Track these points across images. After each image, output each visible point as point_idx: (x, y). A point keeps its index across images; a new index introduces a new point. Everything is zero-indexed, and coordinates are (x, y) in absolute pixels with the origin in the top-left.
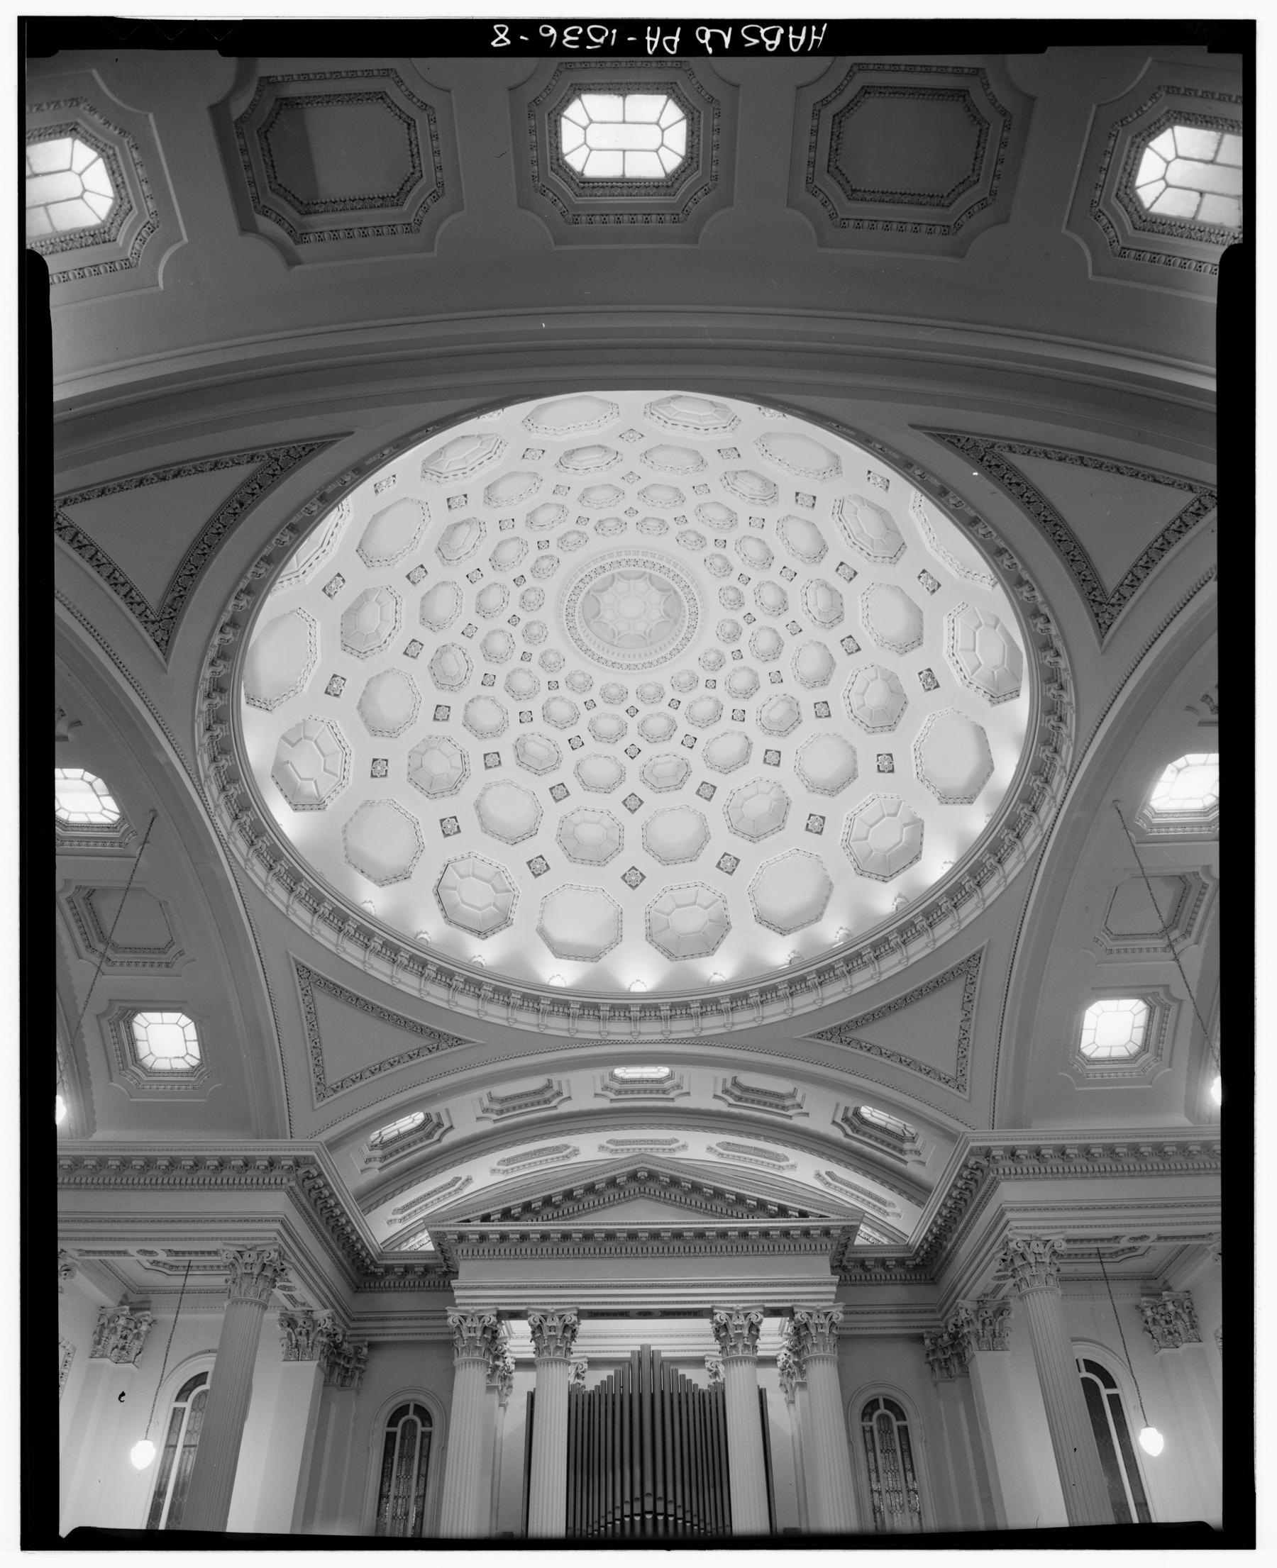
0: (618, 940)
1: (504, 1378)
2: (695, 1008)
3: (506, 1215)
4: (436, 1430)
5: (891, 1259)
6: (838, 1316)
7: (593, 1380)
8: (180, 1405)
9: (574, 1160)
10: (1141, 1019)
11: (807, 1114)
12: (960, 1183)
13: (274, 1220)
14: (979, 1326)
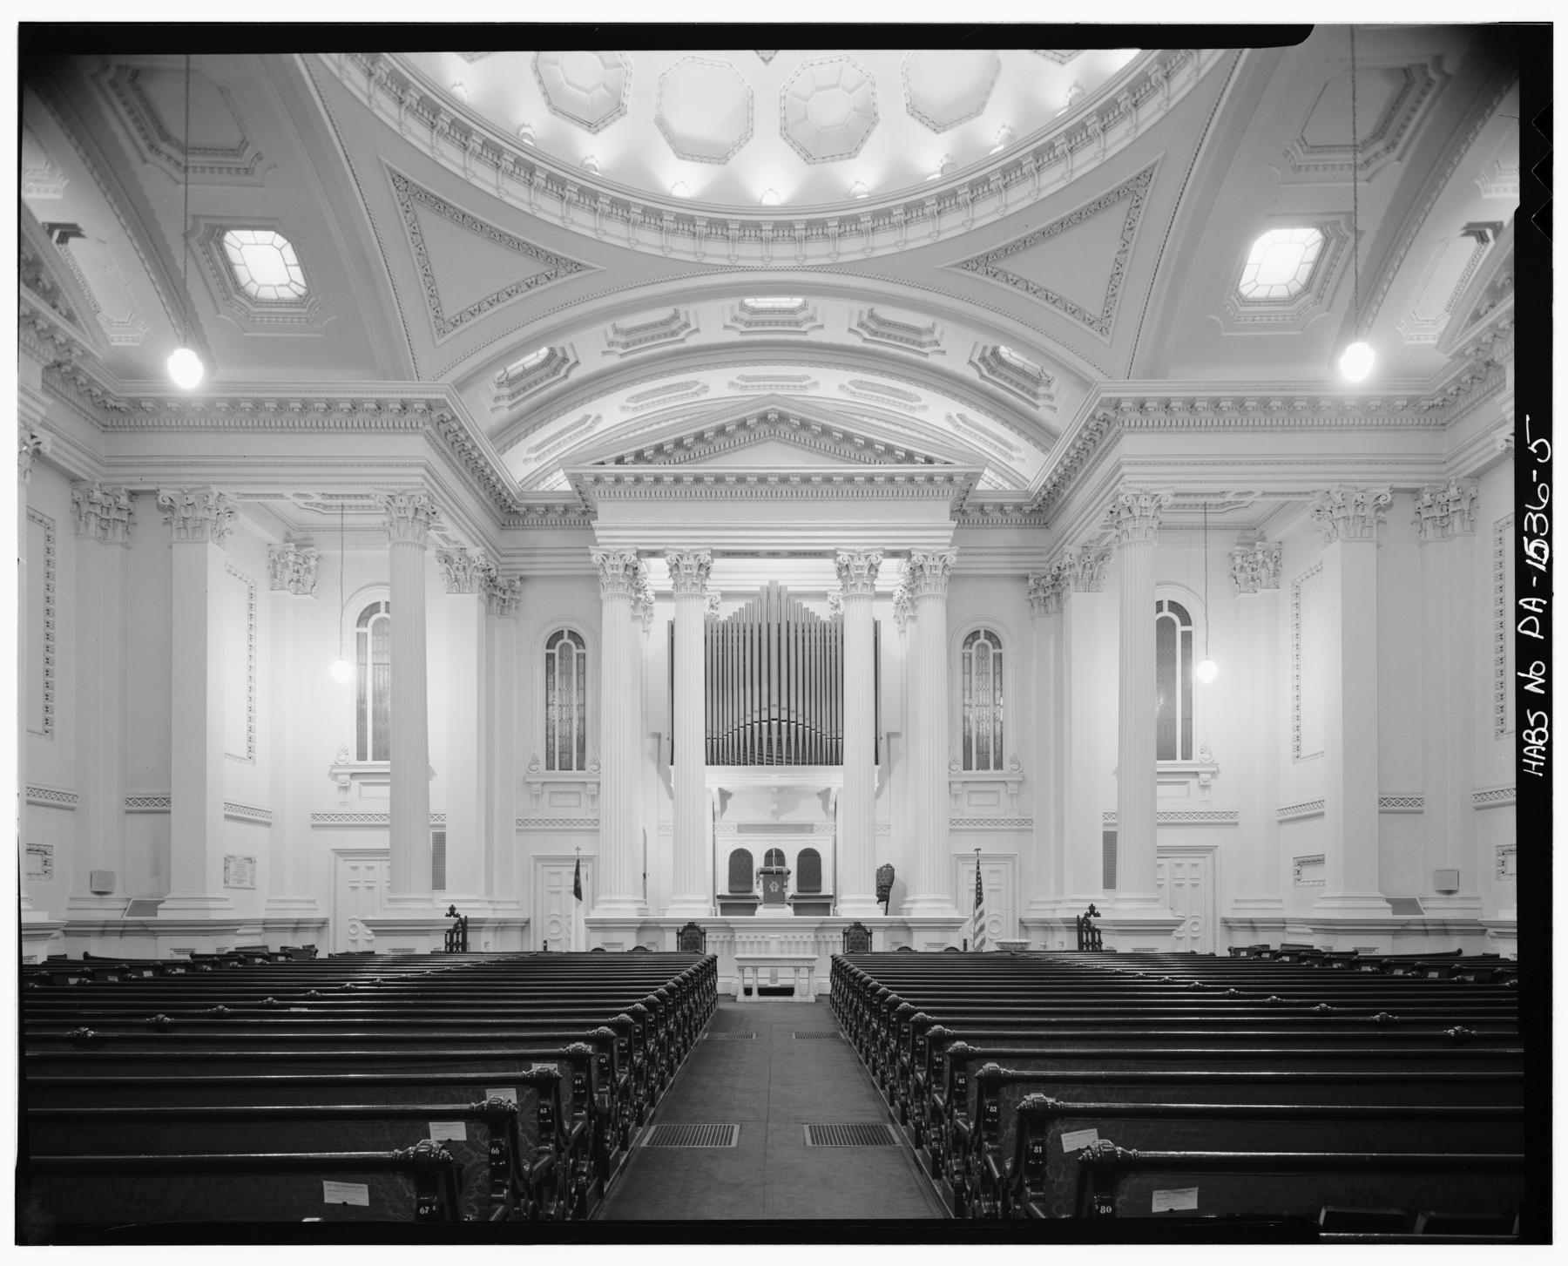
0: (747, 136)
1: (646, 608)
2: (833, 228)
3: (639, 457)
4: (589, 651)
5: (1008, 504)
6: (952, 559)
7: (727, 611)
8: (362, 630)
9: (703, 397)
10: (1312, 253)
11: (944, 352)
12: (1085, 434)
13: (418, 465)
14: (1079, 569)
